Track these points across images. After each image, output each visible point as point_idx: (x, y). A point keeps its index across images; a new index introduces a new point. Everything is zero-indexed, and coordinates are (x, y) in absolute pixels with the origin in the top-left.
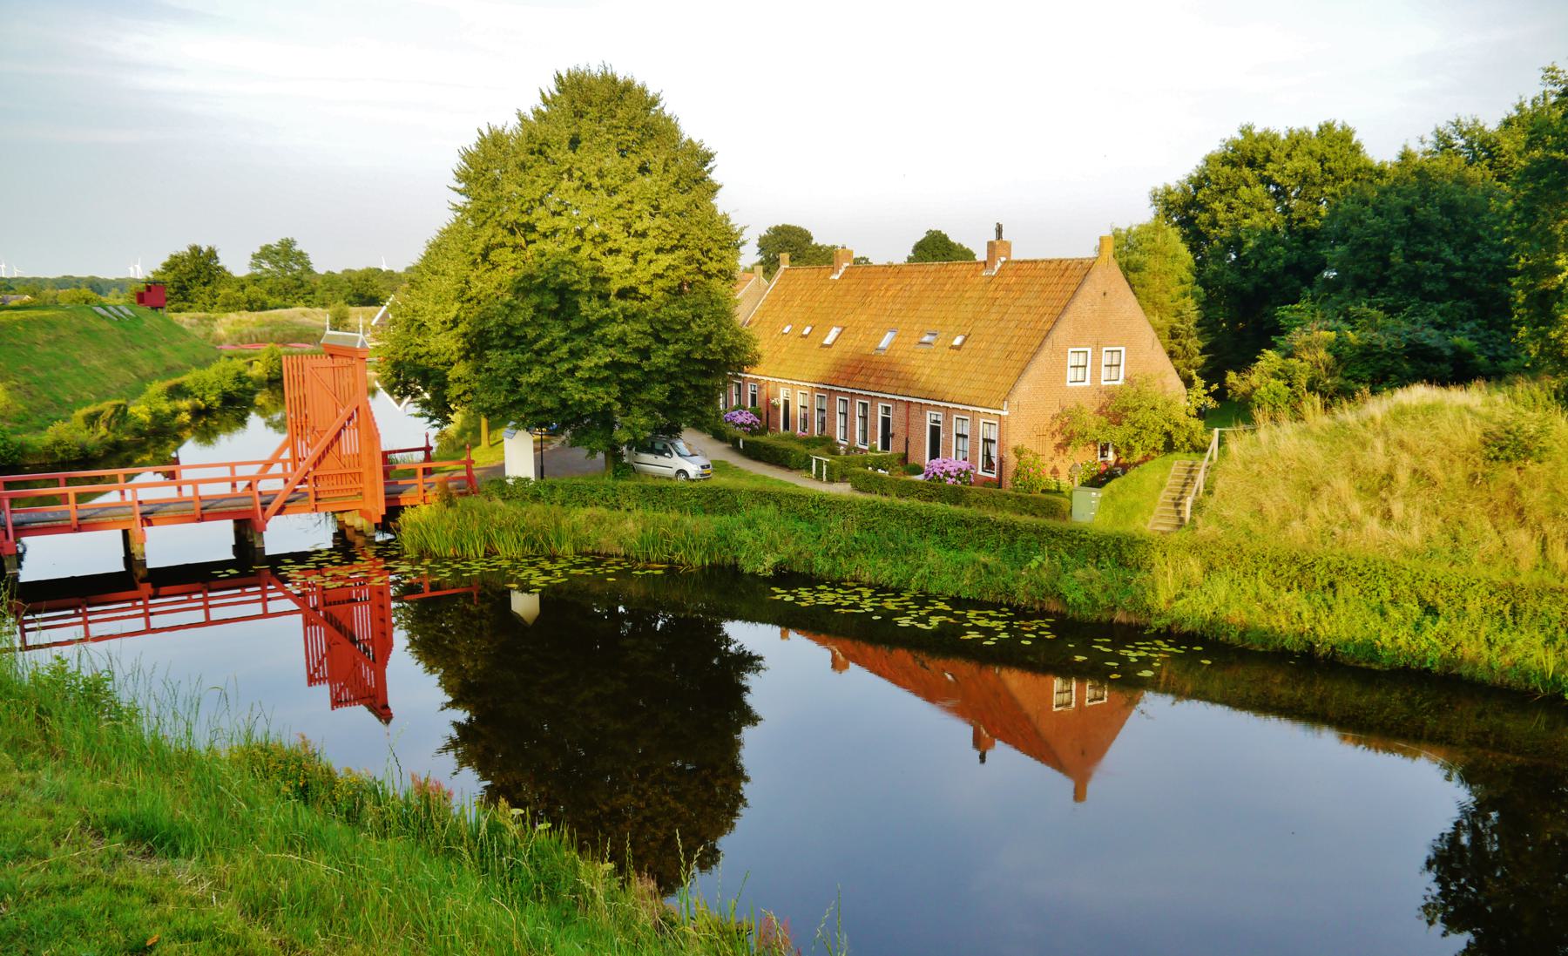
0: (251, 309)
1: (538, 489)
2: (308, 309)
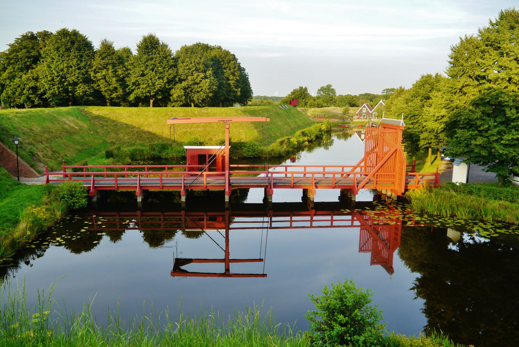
0: (318, 107)
1: (472, 189)
2: (335, 108)
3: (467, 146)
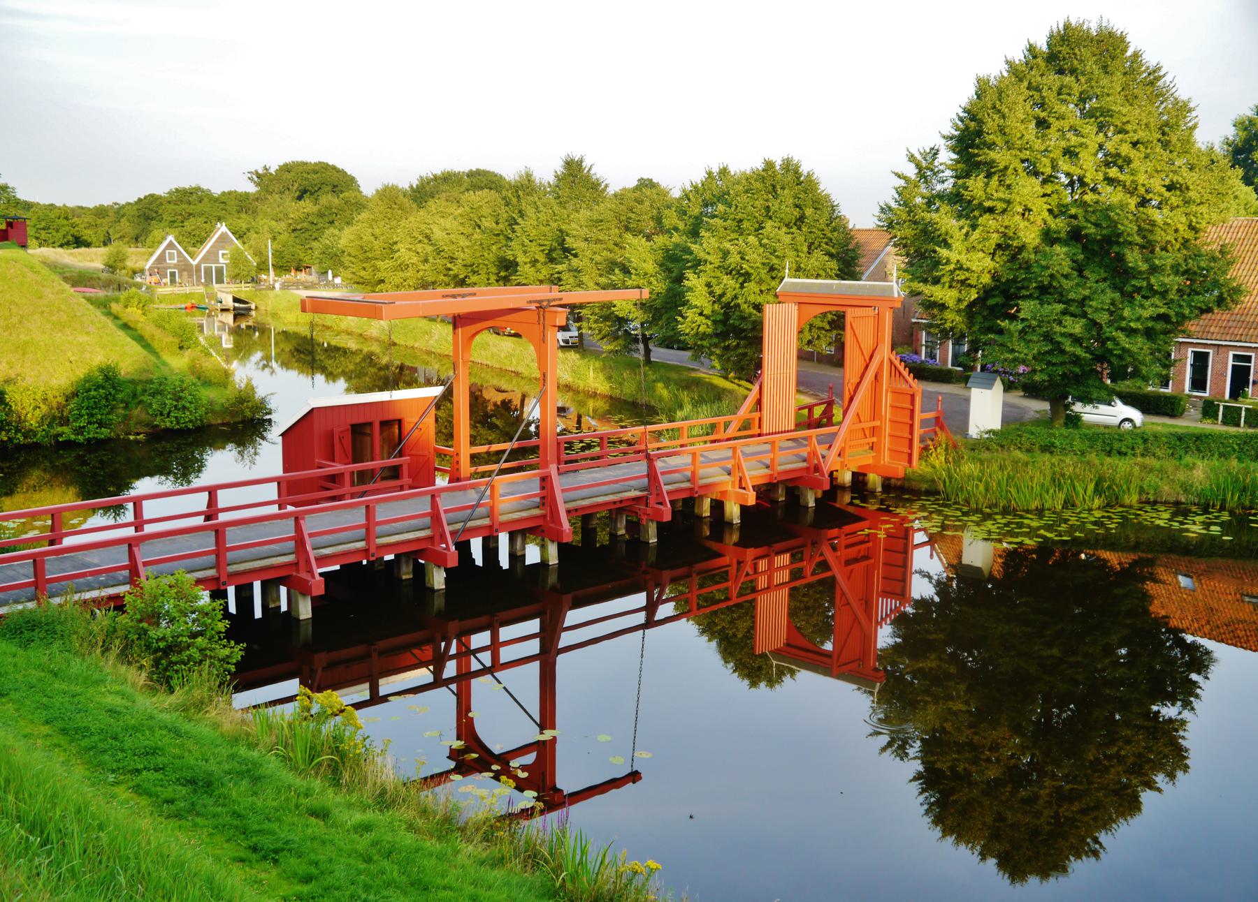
3: (636, 340)
